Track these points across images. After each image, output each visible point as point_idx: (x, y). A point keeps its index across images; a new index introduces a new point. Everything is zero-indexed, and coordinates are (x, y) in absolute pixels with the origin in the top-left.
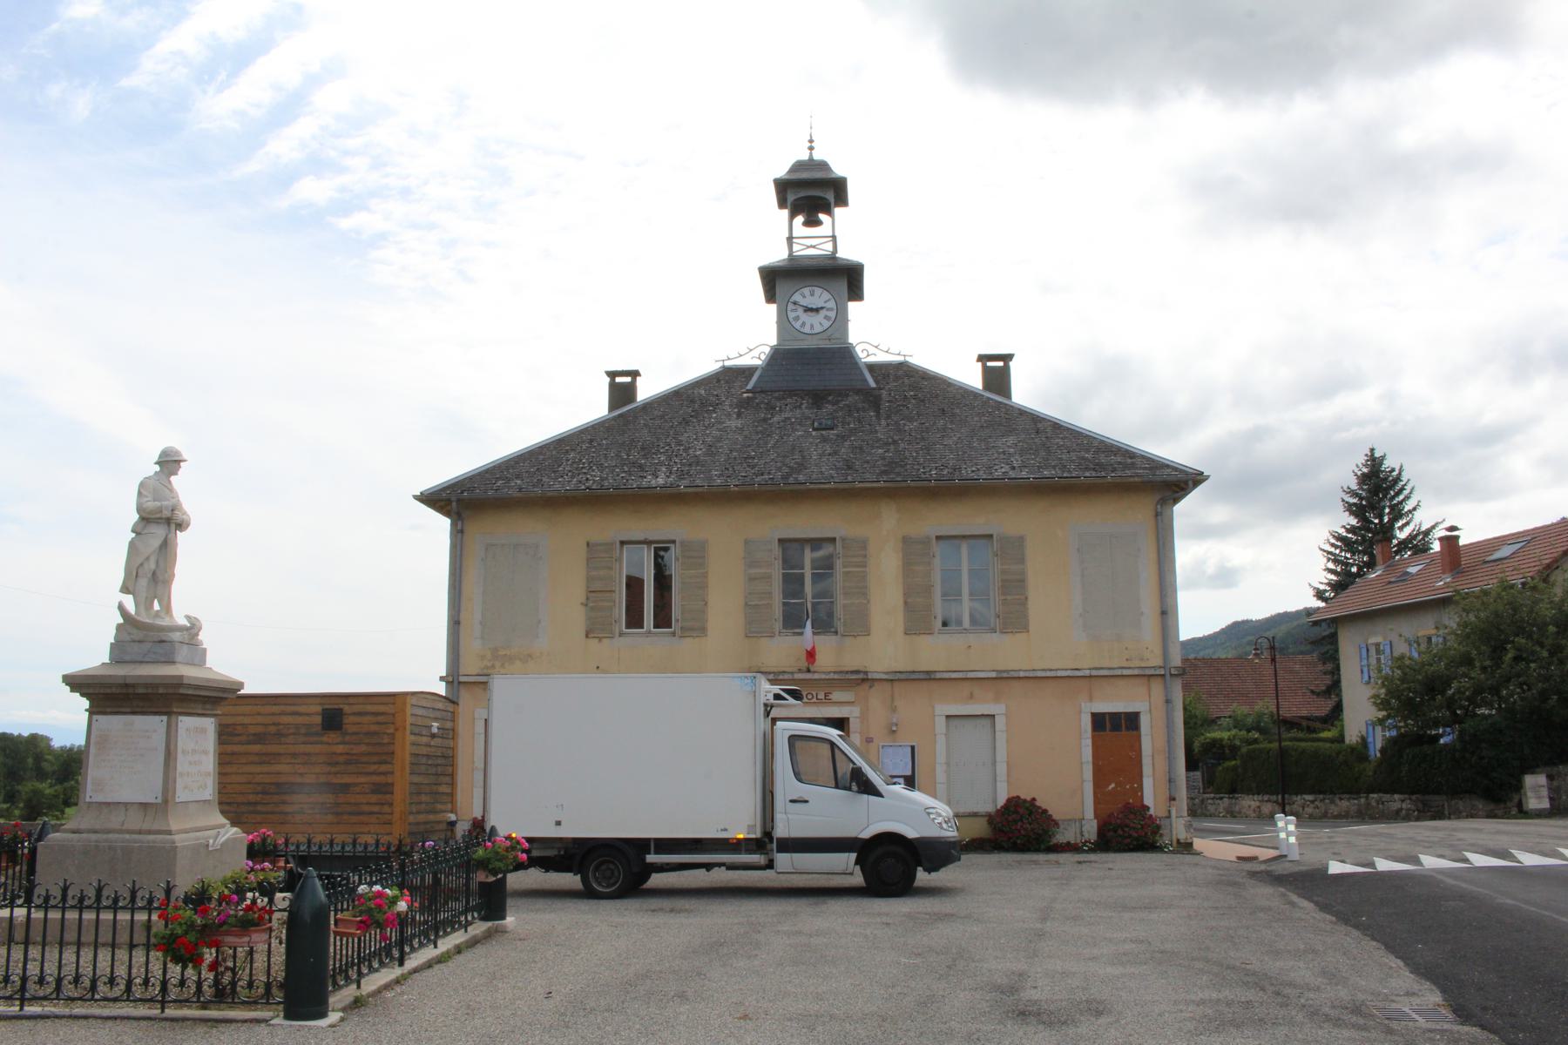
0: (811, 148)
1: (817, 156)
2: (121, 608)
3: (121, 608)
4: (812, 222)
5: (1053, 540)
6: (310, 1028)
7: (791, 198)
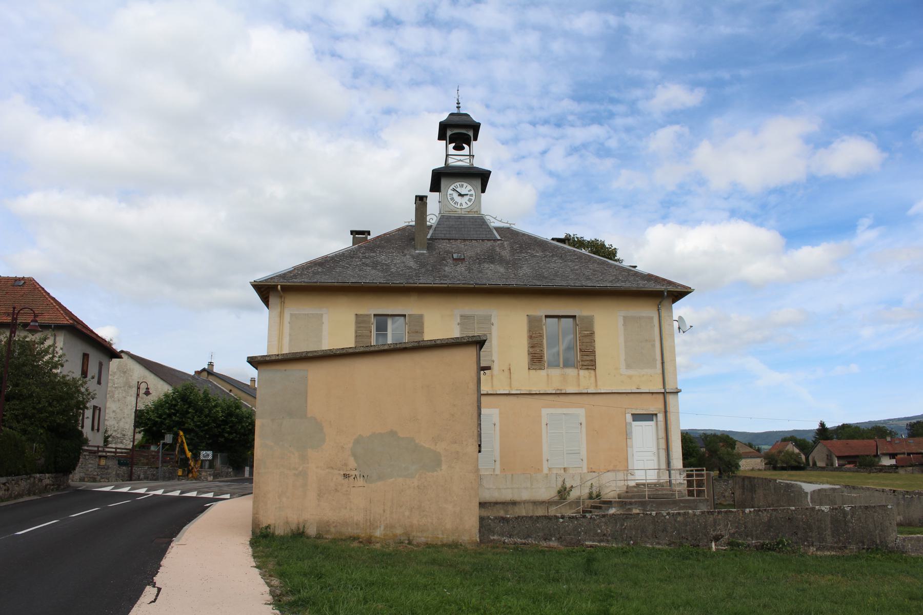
0: (458, 107)
4: (459, 148)
5: (610, 324)
6: (609, 264)
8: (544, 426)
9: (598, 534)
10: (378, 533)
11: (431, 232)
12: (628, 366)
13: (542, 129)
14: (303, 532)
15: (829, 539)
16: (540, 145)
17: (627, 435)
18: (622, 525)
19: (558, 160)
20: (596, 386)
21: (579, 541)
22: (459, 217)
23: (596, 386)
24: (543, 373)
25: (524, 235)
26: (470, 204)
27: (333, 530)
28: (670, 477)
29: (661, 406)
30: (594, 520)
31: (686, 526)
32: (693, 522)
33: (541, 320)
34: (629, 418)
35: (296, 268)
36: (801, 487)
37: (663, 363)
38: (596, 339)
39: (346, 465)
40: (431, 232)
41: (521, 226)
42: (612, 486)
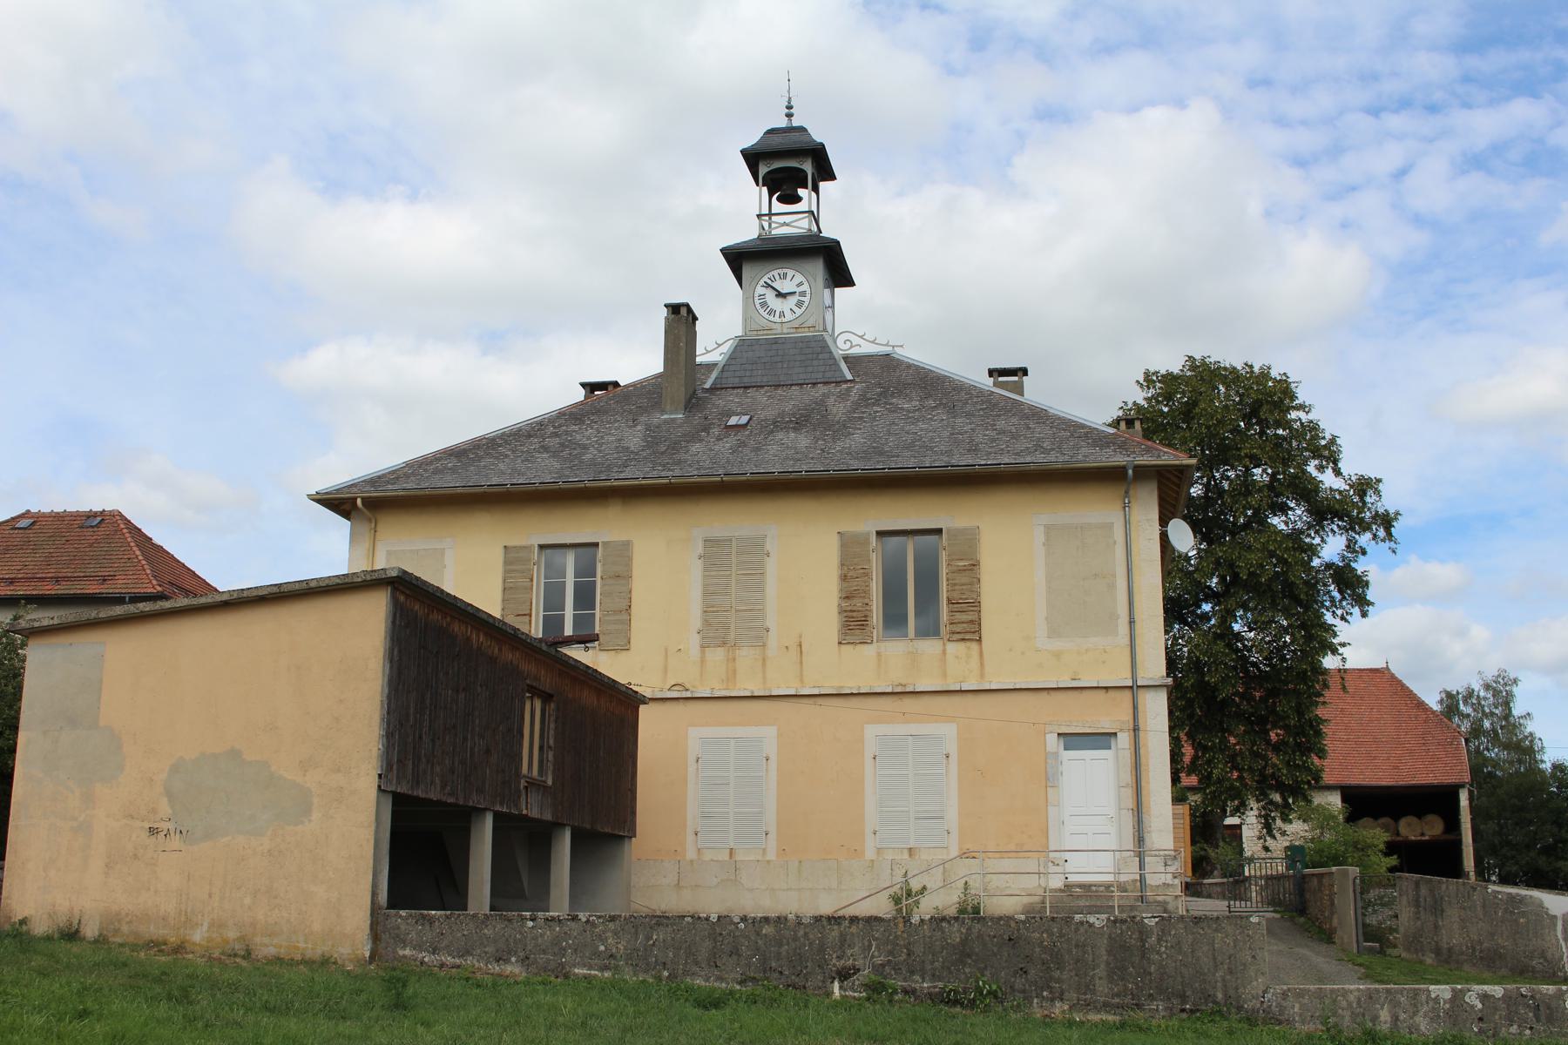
0: (789, 116)
1: (796, 122)
7: (763, 170)
8: (868, 761)
9: (597, 954)
10: (198, 936)
12: (1054, 633)
13: (1394, 122)
14: (77, 931)
15: (1102, 987)
16: (1390, 157)
17: (1048, 779)
18: (649, 938)
19: (1435, 187)
20: (982, 675)
21: (562, 965)
22: (776, 341)
23: (982, 675)
24: (868, 651)
25: (909, 366)
26: (799, 311)
27: (125, 928)
28: (1142, 866)
29: (1127, 717)
30: (594, 925)
31: (781, 945)
32: (795, 939)
33: (867, 541)
34: (1052, 741)
35: (409, 465)
36: (1541, 905)
37: (1132, 622)
39: (154, 811)
40: (714, 375)
42: (1010, 891)
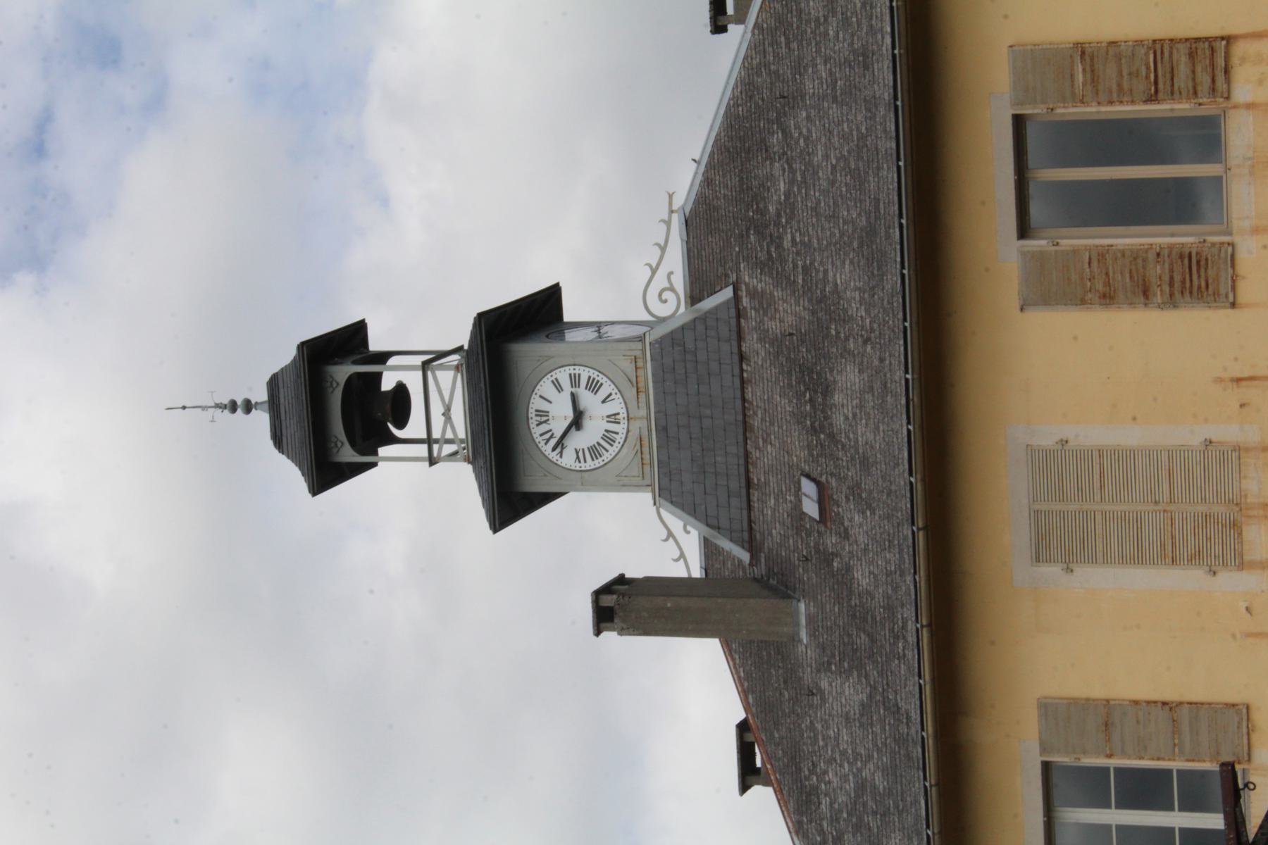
0: (248, 407)
1: (260, 394)
2: (623, 605)
3: (623, 605)
7: (348, 454)
11: (725, 544)
22: (663, 430)
26: (607, 388)
38: (1084, 696)
40: (725, 544)
41: (682, 180)
